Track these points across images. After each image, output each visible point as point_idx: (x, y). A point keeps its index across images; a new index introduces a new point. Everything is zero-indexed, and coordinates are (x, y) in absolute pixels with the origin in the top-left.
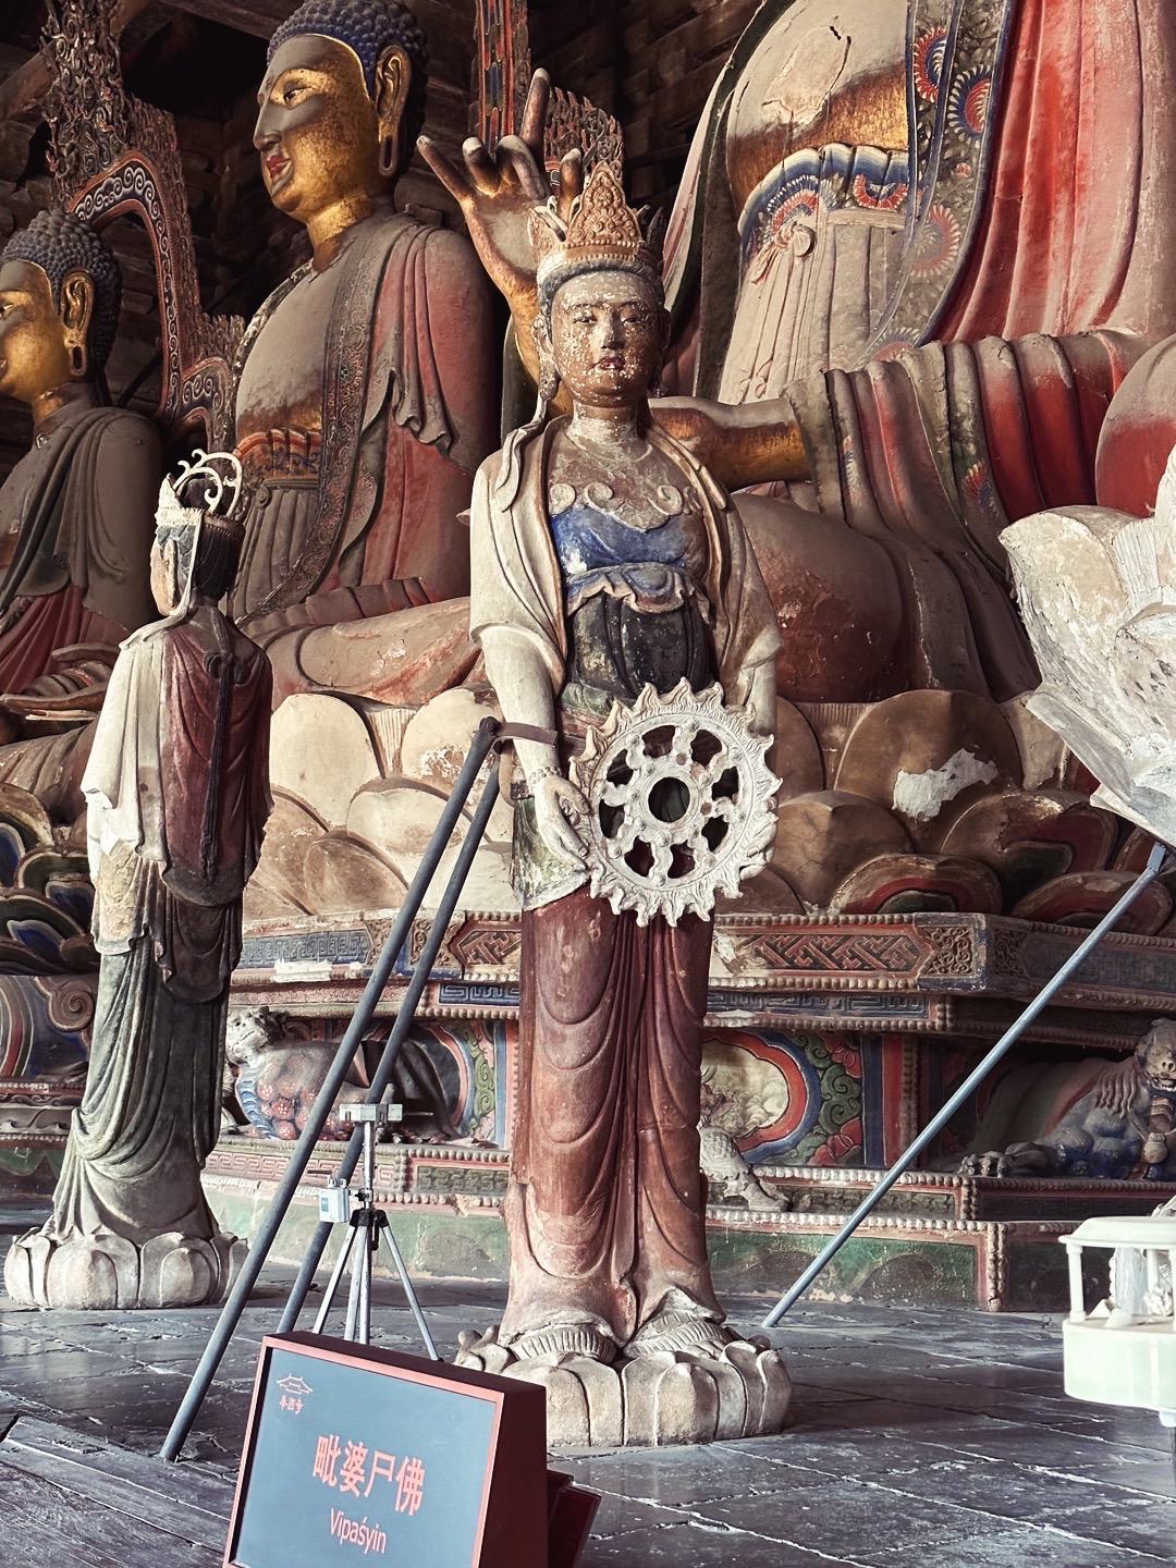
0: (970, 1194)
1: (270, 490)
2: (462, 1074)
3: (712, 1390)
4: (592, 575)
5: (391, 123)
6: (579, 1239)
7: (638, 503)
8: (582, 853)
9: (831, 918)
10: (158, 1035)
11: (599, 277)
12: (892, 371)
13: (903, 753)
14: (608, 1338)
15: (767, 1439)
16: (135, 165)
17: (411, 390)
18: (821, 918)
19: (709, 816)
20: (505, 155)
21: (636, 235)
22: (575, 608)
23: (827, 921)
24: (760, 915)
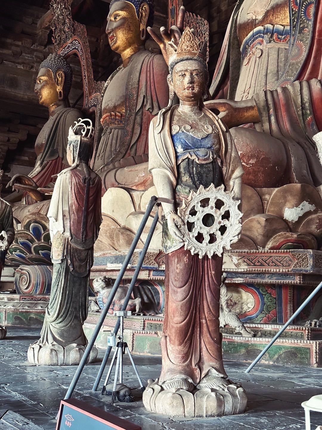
0: (308, 332)
1: (111, 130)
2: (160, 296)
3: (222, 400)
4: (185, 152)
5: (144, 25)
6: (182, 353)
7: (199, 131)
8: (182, 237)
9: (266, 251)
10: (69, 287)
11: (187, 62)
12: (285, 90)
13: (287, 202)
14: (191, 383)
15: (240, 415)
16: (75, 40)
17: (150, 100)
18: (263, 251)
19: (221, 225)
20: (172, 31)
21: (198, 49)
22: (180, 162)
23: (265, 252)
24: (245, 250)
